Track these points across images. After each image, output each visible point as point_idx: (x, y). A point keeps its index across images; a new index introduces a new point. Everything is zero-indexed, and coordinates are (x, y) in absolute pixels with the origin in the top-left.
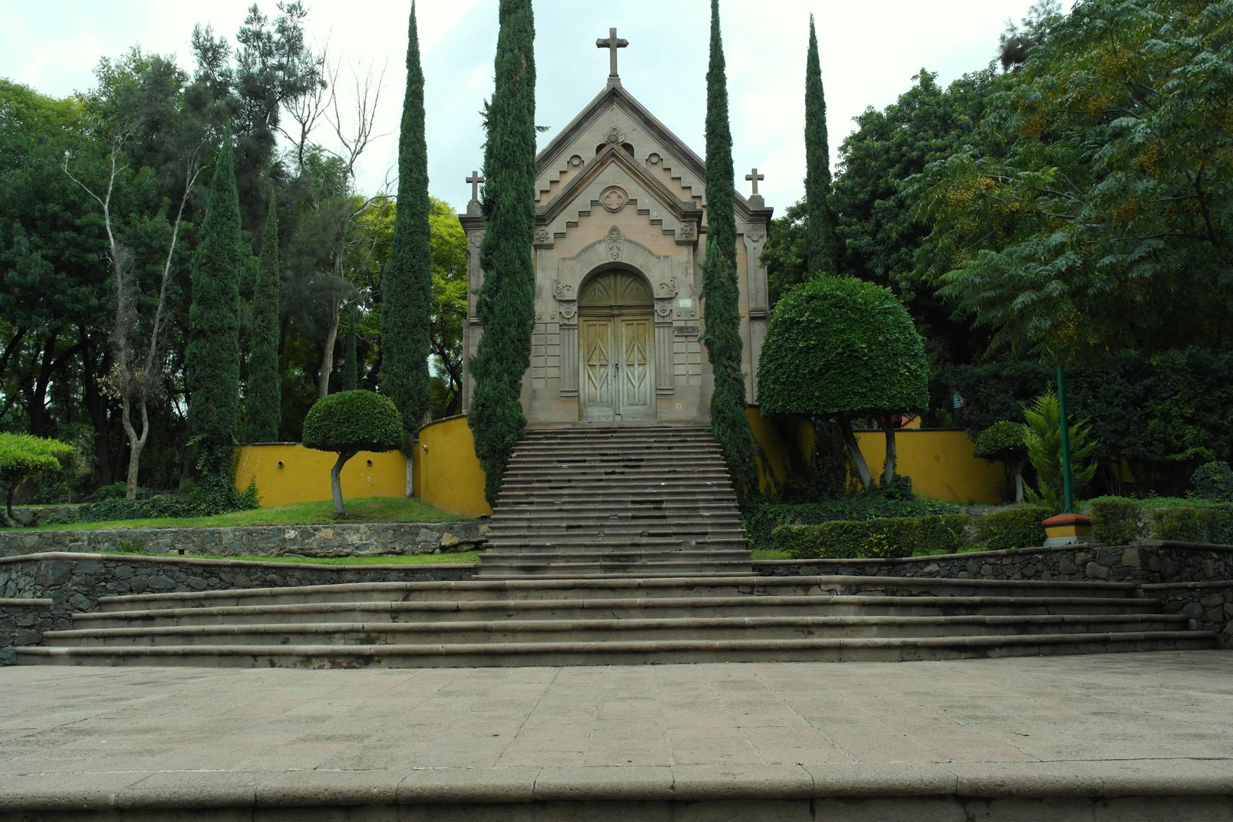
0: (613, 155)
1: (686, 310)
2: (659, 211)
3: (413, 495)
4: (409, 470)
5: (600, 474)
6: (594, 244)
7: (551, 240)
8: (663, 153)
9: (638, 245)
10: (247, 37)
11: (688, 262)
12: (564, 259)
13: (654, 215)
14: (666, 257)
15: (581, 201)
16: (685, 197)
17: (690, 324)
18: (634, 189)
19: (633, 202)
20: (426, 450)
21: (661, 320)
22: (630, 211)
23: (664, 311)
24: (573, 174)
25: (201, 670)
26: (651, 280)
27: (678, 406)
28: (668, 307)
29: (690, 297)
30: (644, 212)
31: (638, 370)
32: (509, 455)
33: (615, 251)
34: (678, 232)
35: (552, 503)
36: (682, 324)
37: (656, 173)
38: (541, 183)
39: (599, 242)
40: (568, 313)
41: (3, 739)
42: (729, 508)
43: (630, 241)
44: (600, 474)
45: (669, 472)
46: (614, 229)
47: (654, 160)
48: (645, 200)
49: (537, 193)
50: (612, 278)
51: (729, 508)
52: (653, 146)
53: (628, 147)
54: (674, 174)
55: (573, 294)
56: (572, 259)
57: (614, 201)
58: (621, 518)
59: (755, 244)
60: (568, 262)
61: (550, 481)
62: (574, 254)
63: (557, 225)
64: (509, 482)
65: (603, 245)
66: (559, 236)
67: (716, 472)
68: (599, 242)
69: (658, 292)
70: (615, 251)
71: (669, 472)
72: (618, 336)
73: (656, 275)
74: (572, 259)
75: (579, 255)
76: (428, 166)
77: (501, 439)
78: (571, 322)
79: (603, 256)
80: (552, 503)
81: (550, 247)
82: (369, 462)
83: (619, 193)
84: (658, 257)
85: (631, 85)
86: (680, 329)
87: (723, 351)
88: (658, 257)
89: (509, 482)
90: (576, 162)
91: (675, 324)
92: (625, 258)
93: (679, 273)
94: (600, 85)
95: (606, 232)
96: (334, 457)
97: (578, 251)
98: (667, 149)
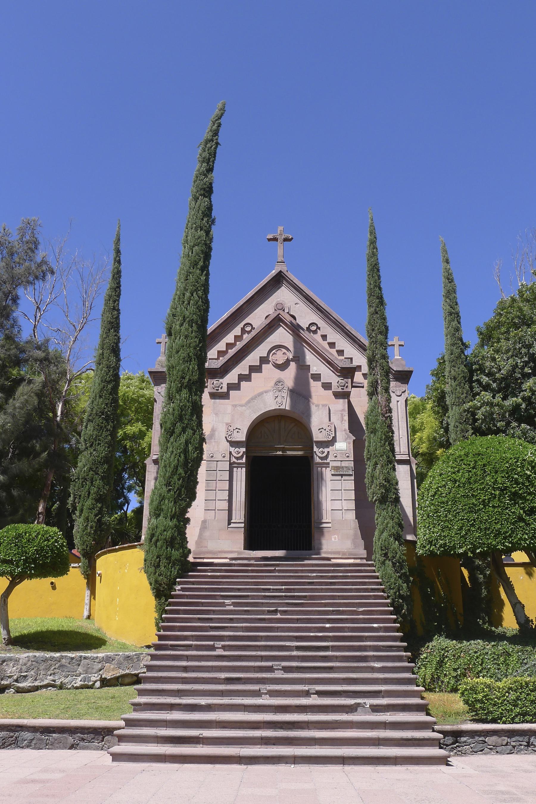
3: (89, 617)
6: (260, 394)
8: (321, 323)
11: (343, 410)
17: (344, 464)
20: (100, 575)
23: (323, 452)
24: (247, 338)
25: (239, 515)
29: (345, 440)
34: (334, 385)
36: (338, 464)
38: (212, 353)
41: (4, 682)
54: (329, 340)
55: (242, 437)
59: (398, 398)
60: (238, 408)
62: (243, 402)
63: (232, 377)
67: (185, 638)
69: (317, 436)
74: (241, 406)
75: (249, 402)
86: (337, 468)
91: (332, 464)
95: (272, 383)
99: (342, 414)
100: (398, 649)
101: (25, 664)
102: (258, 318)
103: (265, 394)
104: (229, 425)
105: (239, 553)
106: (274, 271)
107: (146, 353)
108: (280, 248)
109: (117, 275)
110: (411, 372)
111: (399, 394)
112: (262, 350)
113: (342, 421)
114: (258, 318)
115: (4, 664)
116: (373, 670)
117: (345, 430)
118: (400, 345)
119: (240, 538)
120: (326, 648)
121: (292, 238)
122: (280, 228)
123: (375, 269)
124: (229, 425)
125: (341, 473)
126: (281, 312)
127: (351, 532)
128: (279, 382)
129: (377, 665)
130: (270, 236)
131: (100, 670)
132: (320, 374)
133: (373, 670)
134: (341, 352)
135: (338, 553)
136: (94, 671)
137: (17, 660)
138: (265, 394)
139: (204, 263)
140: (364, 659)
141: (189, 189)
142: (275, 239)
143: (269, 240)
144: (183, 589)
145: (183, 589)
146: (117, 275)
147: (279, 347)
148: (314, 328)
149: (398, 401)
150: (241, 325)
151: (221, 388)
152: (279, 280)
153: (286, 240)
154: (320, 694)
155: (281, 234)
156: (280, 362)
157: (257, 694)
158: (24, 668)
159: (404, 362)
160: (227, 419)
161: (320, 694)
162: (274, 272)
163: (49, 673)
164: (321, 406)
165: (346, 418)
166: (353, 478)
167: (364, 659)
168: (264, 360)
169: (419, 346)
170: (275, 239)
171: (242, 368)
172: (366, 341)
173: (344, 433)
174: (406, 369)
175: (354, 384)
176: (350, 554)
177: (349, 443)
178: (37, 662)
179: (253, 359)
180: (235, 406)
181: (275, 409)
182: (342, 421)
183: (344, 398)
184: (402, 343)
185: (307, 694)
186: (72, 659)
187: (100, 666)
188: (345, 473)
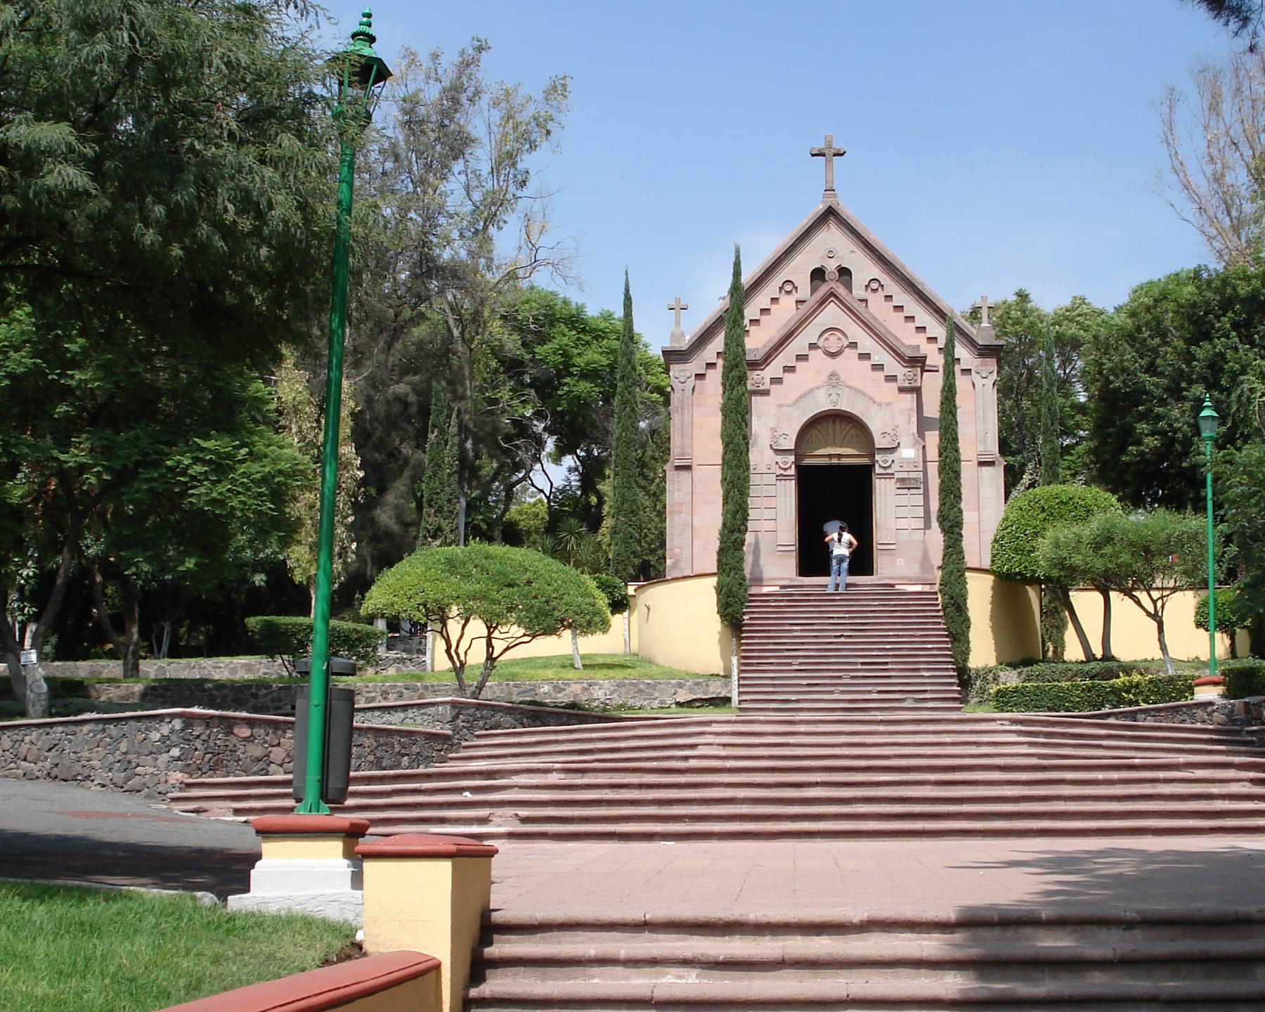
0: (832, 294)
1: (909, 461)
2: (880, 355)
6: (811, 391)
7: (767, 386)
8: (885, 279)
9: (858, 391)
11: (912, 409)
12: (781, 406)
13: (876, 359)
15: (798, 344)
17: (912, 475)
18: (856, 332)
19: (853, 345)
21: (882, 471)
22: (850, 354)
26: (872, 429)
27: (900, 562)
28: (890, 457)
30: (865, 356)
33: (834, 397)
36: (905, 475)
40: (785, 463)
42: (947, 670)
43: (850, 387)
44: (830, 637)
46: (833, 375)
47: (874, 285)
48: (867, 343)
49: (746, 322)
50: (830, 423)
51: (947, 670)
52: (875, 271)
53: (844, 272)
57: (833, 344)
58: (852, 677)
60: (785, 408)
62: (791, 401)
63: (774, 369)
64: (747, 638)
65: (823, 391)
66: (776, 381)
69: (880, 442)
70: (834, 397)
73: (877, 424)
74: (788, 406)
75: (796, 402)
78: (788, 473)
79: (823, 404)
80: (790, 664)
81: (766, 393)
83: (839, 335)
84: (880, 405)
85: (847, 209)
88: (880, 405)
89: (747, 638)
90: (788, 287)
91: (897, 475)
92: (844, 406)
93: (901, 421)
94: (821, 207)
95: (824, 377)
98: (885, 271)
104: (774, 430)
105: (790, 579)
119: (791, 563)
120: (887, 663)
124: (774, 430)
129: (926, 674)
133: (923, 677)
135: (904, 578)
140: (918, 670)
144: (751, 619)
145: (751, 619)
148: (874, 285)
152: (830, 214)
154: (879, 692)
157: (832, 692)
160: (771, 423)
161: (879, 692)
165: (914, 419)
176: (918, 579)
185: (870, 692)
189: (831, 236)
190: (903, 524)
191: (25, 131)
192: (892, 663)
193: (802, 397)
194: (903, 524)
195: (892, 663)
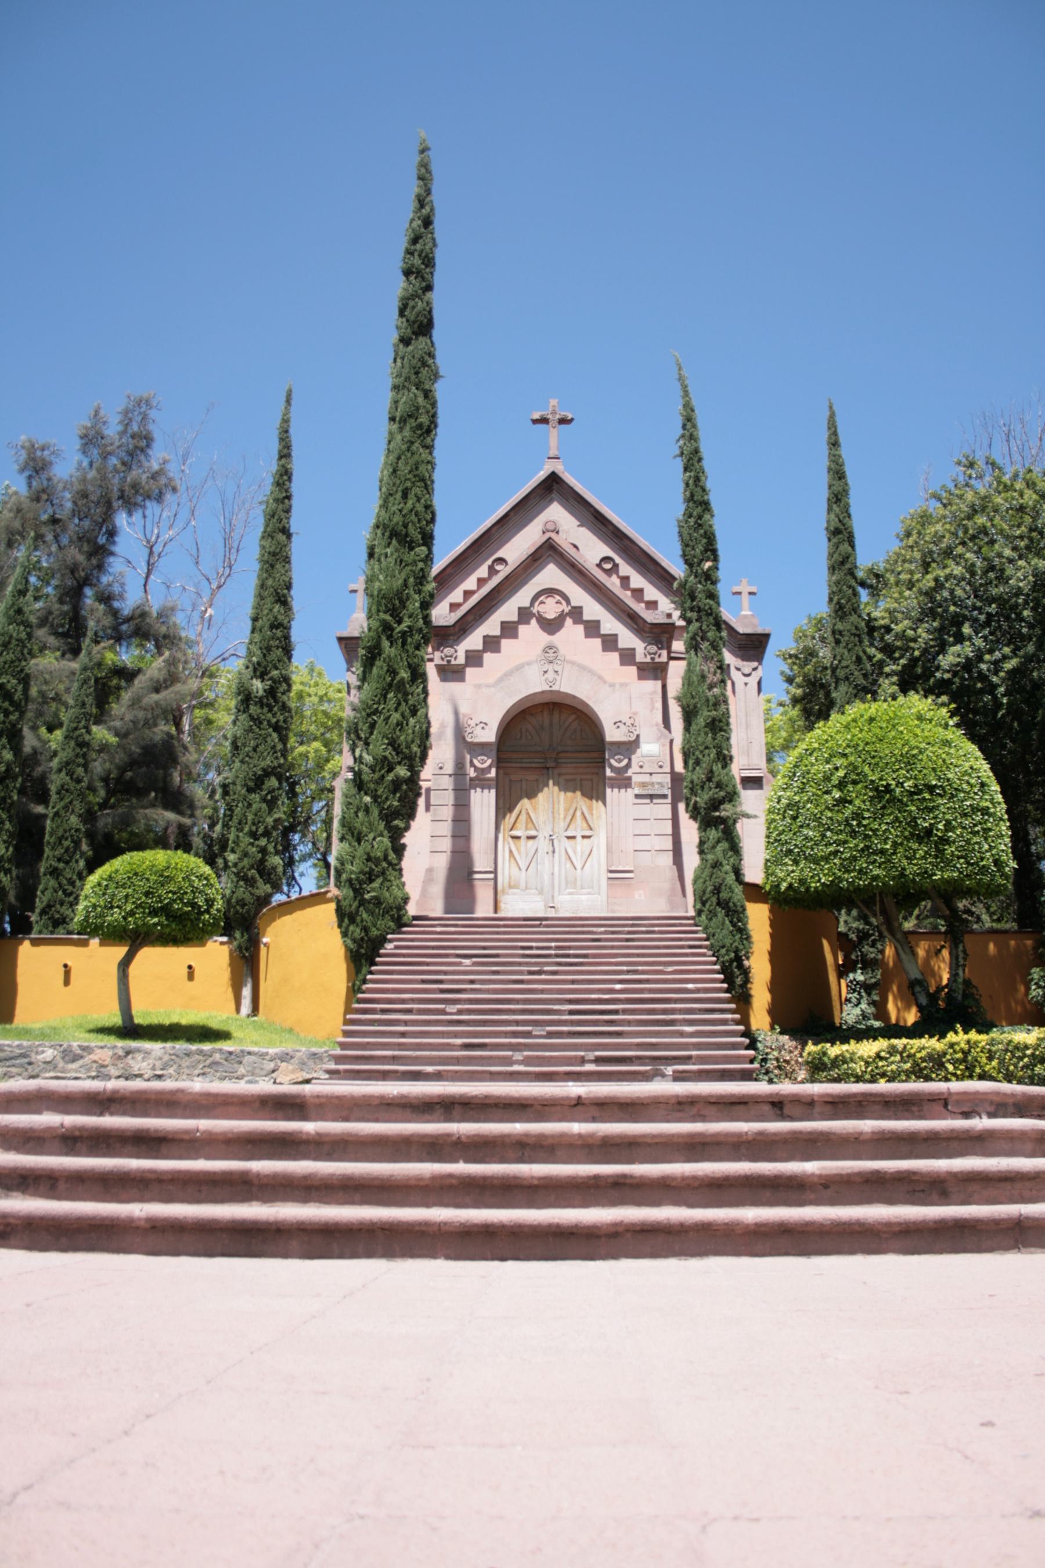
2: (610, 624)
4: (247, 992)
5: (521, 973)
6: (519, 668)
9: (582, 668)
10: (91, 439)
11: (654, 692)
14: (623, 685)
16: (650, 617)
17: (656, 778)
18: (579, 596)
20: (265, 945)
27: (639, 895)
31: (581, 845)
32: (382, 946)
33: (551, 675)
34: (640, 657)
35: (443, 1012)
36: (646, 778)
37: (613, 583)
39: (528, 664)
42: (724, 1022)
43: (573, 663)
44: (521, 973)
45: (628, 972)
47: (608, 566)
48: (593, 610)
51: (724, 1022)
55: (489, 735)
56: (488, 686)
57: (550, 608)
59: (747, 679)
61: (441, 982)
63: (473, 641)
68: (528, 664)
69: (612, 734)
70: (551, 675)
71: (628, 972)
72: (550, 806)
74: (488, 686)
75: (500, 680)
76: (496, 1264)
77: (371, 924)
82: (191, 976)
84: (612, 685)
87: (707, 797)
88: (612, 685)
96: (122, 951)
97: (499, 674)
99: (652, 699)
100: (734, 1046)
101: (160, 1059)
102: (517, 549)
103: (526, 667)
106: (542, 473)
107: (333, 604)
108: (553, 435)
109: (284, 477)
110: (766, 636)
111: (747, 672)
112: (522, 597)
113: (652, 710)
114: (517, 549)
115: (130, 1057)
116: (682, 1034)
117: (657, 725)
118: (750, 593)
120: (616, 1012)
121: (572, 420)
122: (553, 402)
123: (692, 460)
125: (651, 792)
126: (553, 535)
127: (666, 886)
128: (550, 647)
130: (536, 416)
131: (273, 1071)
132: (616, 635)
133: (682, 1034)
134: (652, 605)
136: (264, 1073)
137: (147, 1053)
138: (526, 667)
139: (62, 581)
140: (672, 1023)
141: (389, 327)
142: (544, 421)
143: (535, 422)
146: (284, 477)
147: (550, 592)
149: (746, 684)
150: (489, 562)
151: (456, 658)
152: (552, 487)
153: (563, 421)
155: (554, 413)
156: (551, 615)
158: (158, 1064)
159: (755, 621)
162: (542, 475)
163: (197, 1072)
164: (617, 686)
166: (669, 800)
167: (672, 1023)
168: (525, 615)
169: (775, 590)
170: (544, 421)
171: (491, 626)
172: (678, 569)
173: (655, 729)
174: (759, 630)
175: (673, 655)
177: (664, 745)
178: (177, 1056)
179: (508, 611)
180: (478, 686)
181: (543, 692)
182: (652, 710)
183: (656, 678)
184: (753, 589)
186: (231, 1053)
187: (272, 1065)
188: (656, 792)
189: (556, 512)
190: (643, 843)
191: (3, 680)
192: (625, 1012)
193: (507, 675)
194: (643, 843)
195: (625, 1012)
